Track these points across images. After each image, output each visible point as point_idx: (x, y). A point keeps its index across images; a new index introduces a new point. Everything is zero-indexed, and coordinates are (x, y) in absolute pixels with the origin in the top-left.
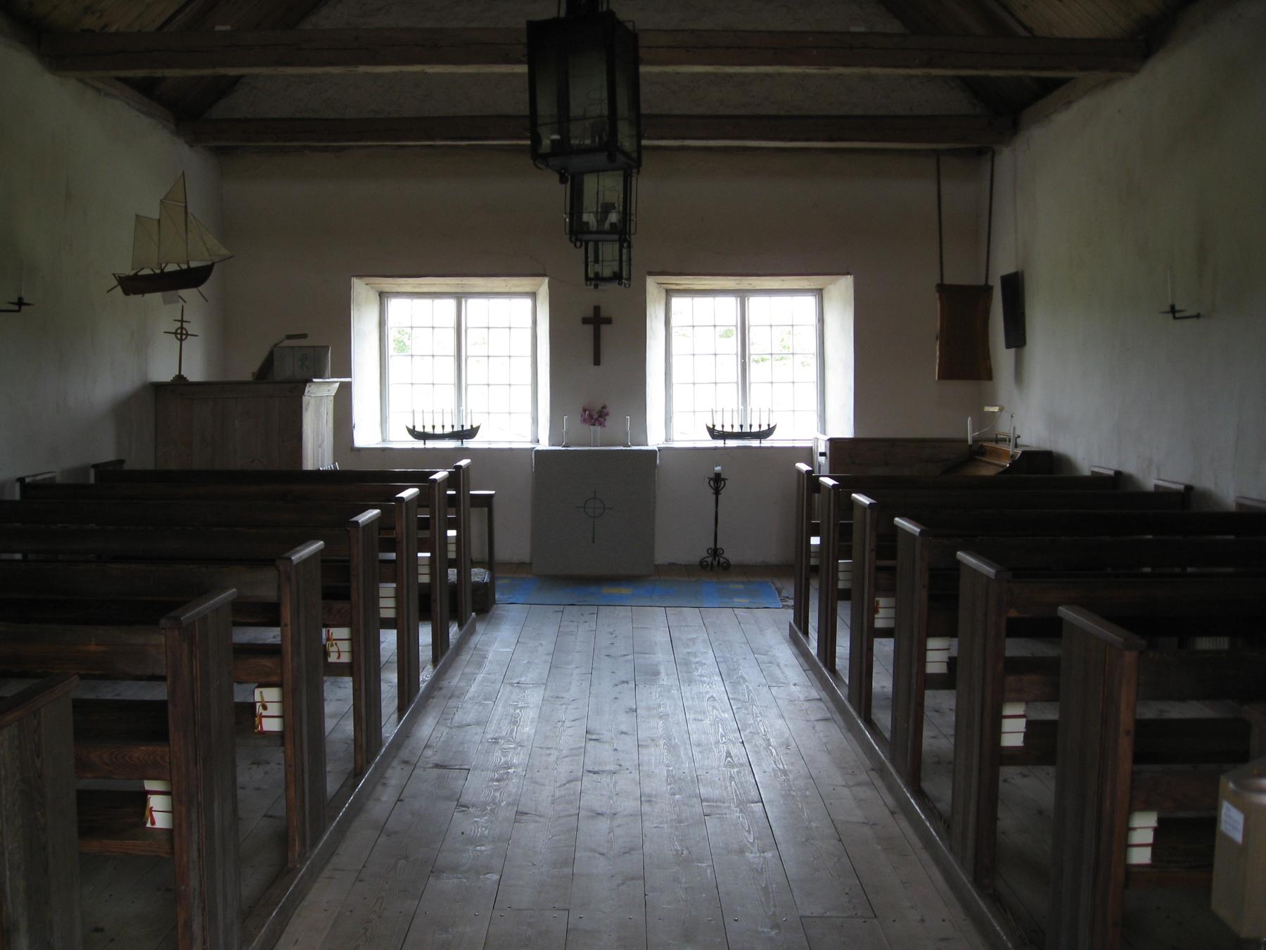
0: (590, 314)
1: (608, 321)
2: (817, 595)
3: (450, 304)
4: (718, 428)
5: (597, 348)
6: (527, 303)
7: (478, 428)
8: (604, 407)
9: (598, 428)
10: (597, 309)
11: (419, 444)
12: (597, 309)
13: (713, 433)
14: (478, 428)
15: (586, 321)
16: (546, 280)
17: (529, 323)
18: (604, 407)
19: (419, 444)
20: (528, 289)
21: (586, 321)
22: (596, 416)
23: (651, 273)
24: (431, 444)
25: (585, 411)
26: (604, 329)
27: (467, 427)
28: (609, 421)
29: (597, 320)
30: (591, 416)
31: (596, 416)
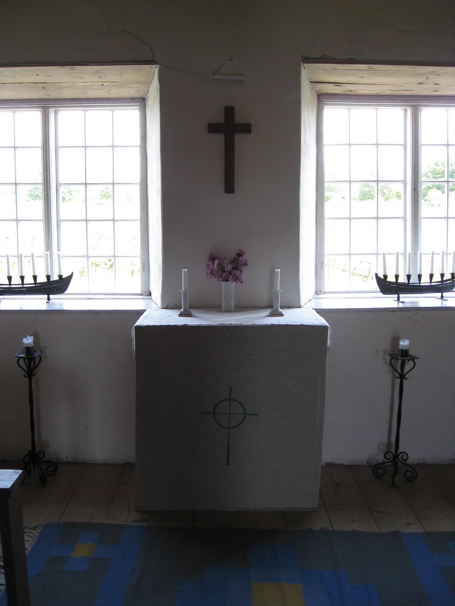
0: (220, 119)
1: (246, 129)
2: (261, 321)
3: (33, 117)
4: (391, 278)
5: (228, 174)
6: (132, 114)
7: (70, 278)
8: (240, 254)
9: (232, 285)
10: (229, 111)
11: (389, 302)
12: (229, 111)
13: (386, 286)
14: (70, 278)
15: (213, 128)
16: (155, 70)
17: (137, 141)
18: (240, 254)
19: (389, 302)
20: (132, 92)
21: (213, 128)
22: (229, 267)
23: (308, 60)
24: (409, 300)
25: (212, 258)
26: (240, 139)
27: (55, 277)
28: (246, 274)
29: (229, 127)
30: (222, 268)
31: (229, 268)
